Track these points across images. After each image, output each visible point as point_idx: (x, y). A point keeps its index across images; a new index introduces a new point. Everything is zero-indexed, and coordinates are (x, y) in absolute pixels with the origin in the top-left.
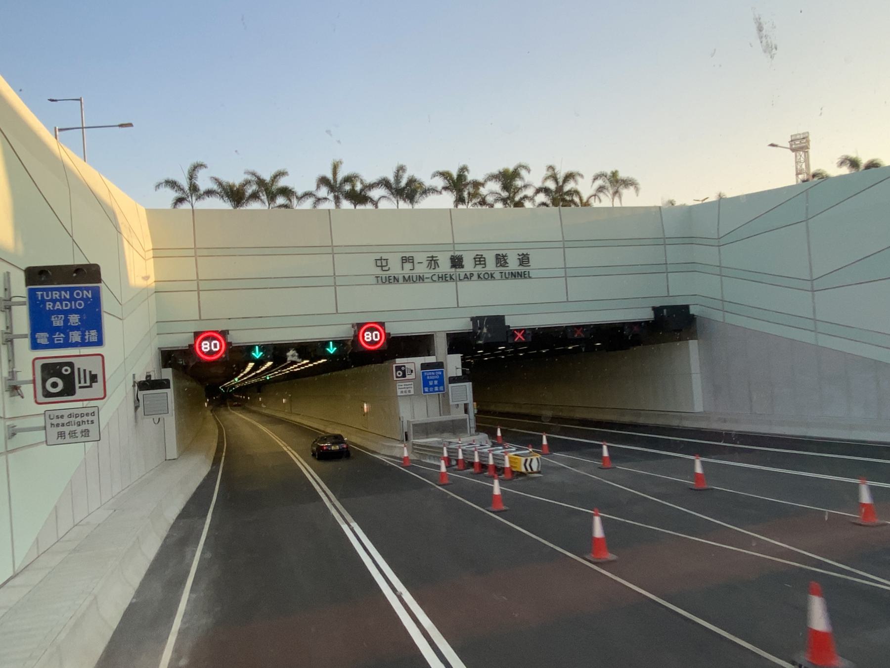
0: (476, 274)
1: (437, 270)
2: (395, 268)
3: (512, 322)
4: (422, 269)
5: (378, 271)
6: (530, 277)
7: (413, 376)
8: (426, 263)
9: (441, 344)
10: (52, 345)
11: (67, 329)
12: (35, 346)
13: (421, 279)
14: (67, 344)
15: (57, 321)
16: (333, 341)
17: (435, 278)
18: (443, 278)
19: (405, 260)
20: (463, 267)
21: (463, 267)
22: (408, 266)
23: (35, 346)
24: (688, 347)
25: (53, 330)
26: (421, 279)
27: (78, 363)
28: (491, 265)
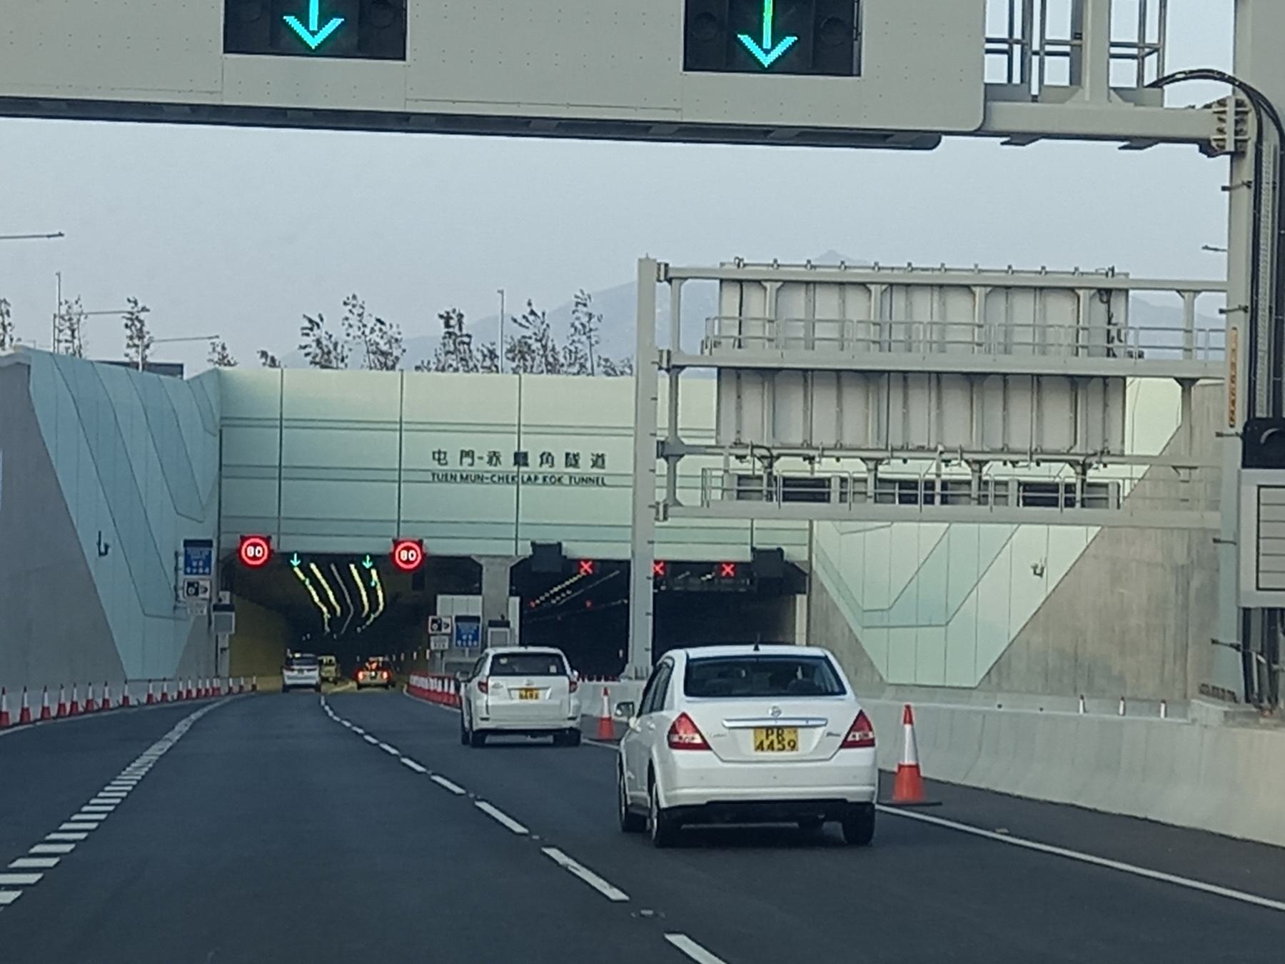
0: (541, 477)
1: (499, 468)
2: (453, 464)
3: (573, 549)
4: (482, 466)
5: (435, 465)
6: (604, 484)
7: (449, 631)
8: (486, 459)
9: (496, 580)
10: (191, 573)
11: (198, 567)
12: (186, 573)
13: (479, 478)
14: (197, 573)
15: (195, 564)
16: (371, 556)
17: (496, 479)
18: (505, 479)
19: (465, 454)
20: (526, 464)
21: (526, 464)
22: (467, 460)
23: (186, 573)
24: (795, 599)
25: (192, 567)
26: (479, 478)
27: (201, 583)
28: (560, 466)
